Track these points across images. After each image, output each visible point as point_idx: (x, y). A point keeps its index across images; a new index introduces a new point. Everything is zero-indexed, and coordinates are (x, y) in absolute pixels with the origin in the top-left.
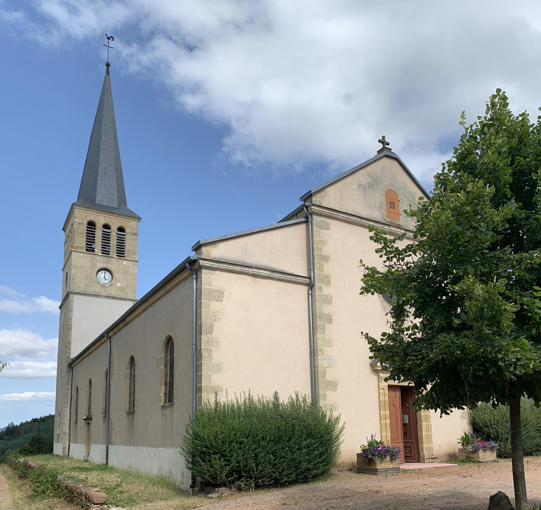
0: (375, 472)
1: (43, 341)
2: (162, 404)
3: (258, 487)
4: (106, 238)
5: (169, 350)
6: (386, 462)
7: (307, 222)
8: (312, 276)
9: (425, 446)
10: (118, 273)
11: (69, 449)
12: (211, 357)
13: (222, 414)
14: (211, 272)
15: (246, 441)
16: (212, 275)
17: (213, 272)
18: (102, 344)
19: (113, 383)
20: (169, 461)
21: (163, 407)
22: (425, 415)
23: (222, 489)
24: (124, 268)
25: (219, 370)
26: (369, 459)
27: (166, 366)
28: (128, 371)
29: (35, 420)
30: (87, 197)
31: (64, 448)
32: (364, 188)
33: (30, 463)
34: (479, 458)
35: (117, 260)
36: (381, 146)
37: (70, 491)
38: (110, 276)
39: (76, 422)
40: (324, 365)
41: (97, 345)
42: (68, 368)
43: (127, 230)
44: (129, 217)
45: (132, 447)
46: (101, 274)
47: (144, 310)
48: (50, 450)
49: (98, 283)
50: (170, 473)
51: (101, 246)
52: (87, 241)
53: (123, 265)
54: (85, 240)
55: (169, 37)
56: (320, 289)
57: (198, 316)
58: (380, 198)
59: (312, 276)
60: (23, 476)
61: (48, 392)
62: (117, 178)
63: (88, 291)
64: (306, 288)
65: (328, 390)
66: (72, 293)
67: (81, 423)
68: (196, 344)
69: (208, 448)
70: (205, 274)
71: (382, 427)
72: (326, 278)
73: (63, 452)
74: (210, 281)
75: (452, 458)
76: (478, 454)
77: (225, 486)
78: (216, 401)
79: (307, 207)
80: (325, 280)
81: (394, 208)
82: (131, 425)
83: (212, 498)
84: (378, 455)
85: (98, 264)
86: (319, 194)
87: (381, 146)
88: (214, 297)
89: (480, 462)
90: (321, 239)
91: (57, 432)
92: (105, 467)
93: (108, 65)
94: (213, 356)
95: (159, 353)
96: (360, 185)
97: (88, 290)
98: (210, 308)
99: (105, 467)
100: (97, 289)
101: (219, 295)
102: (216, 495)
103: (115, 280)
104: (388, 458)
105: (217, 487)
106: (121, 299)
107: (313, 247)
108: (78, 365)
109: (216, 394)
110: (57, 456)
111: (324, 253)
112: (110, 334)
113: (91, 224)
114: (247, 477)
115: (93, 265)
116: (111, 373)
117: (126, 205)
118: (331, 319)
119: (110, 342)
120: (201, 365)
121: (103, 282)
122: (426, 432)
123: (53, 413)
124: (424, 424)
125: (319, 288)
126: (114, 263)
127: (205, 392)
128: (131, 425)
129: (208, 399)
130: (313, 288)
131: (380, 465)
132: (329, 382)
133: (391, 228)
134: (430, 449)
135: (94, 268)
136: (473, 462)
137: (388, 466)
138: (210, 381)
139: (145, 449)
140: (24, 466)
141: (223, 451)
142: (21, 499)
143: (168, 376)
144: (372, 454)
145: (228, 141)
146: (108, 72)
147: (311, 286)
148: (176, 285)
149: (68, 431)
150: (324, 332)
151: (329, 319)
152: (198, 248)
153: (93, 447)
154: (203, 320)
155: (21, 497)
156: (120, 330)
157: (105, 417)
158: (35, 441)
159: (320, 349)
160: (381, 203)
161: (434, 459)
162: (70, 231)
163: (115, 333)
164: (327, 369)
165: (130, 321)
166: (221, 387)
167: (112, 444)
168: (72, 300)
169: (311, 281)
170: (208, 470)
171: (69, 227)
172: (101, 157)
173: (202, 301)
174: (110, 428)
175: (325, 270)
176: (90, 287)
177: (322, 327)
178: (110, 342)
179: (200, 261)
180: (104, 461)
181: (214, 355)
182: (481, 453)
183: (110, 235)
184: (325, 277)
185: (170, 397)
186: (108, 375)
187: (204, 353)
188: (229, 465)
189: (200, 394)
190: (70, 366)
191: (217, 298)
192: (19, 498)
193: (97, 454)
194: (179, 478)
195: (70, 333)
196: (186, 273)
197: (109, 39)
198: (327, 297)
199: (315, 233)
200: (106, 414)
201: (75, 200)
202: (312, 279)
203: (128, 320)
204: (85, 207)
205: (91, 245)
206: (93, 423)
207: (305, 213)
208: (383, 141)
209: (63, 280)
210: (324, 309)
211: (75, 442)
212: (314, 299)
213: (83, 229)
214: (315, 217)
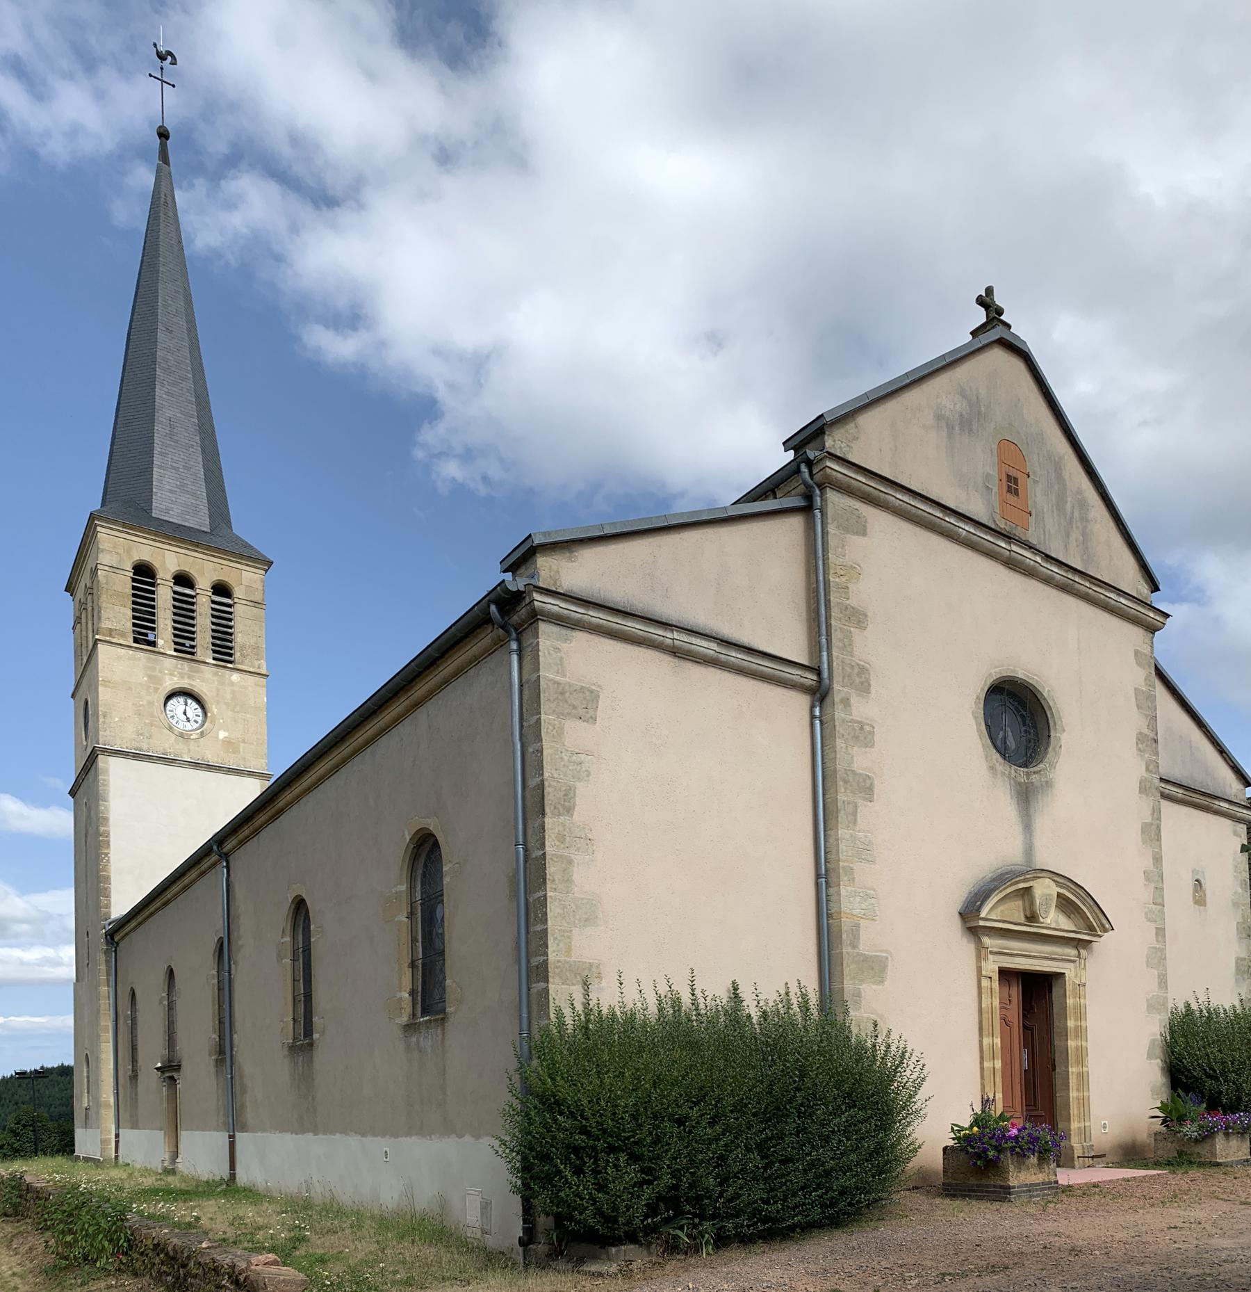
0: (1003, 1194)
1: (17, 900)
2: (405, 1019)
3: (721, 1242)
4: (184, 610)
5: (420, 872)
7: (807, 509)
8: (825, 666)
9: (1075, 1125)
10: (218, 703)
11: (117, 1142)
12: (569, 881)
13: (609, 1040)
14: (564, 631)
15: (694, 1113)
16: (565, 640)
17: (569, 632)
18: (203, 873)
19: (242, 974)
20: (464, 1173)
21: (410, 1028)
22: (1077, 1048)
23: (629, 1249)
24: (233, 692)
25: (589, 920)
26: (978, 1164)
27: (411, 915)
28: (288, 939)
29: (22, 1075)
30: (127, 499)
31: (104, 1142)
32: (950, 428)
33: (28, 1179)
34: (1215, 1155)
35: (215, 669)
36: (980, 316)
37: (173, 1258)
38: (199, 711)
39: (134, 1077)
40: (855, 912)
41: (186, 880)
42: (107, 943)
43: (238, 592)
44: (241, 556)
45: (310, 1135)
46: (177, 705)
47: (336, 768)
48: (66, 1146)
49: (170, 729)
50: (443, 1204)
51: (170, 630)
52: (134, 618)
53: (232, 684)
54: (130, 613)
55: (276, 172)
56: (846, 702)
57: (532, 762)
58: (983, 462)
59: (825, 666)
60: (10, 1211)
61: (32, 1016)
62: (203, 451)
63: (145, 747)
64: (800, 702)
65: (862, 981)
66: (105, 751)
67: (150, 1079)
68: (525, 844)
69: (588, 1134)
70: (548, 638)
71: (987, 1078)
72: (859, 674)
73: (102, 1150)
74: (561, 659)
75: (1130, 1154)
76: (1214, 1145)
77: (632, 1238)
78: (586, 1004)
79: (810, 464)
80: (858, 680)
81: (1016, 493)
82: (305, 1081)
83: (600, 1275)
84: (1012, 1149)
85: (167, 678)
86: (842, 431)
87: (980, 316)
88: (574, 707)
89: (1218, 1165)
91: (82, 1101)
92: (229, 1187)
94: (575, 877)
95: (389, 879)
96: (939, 417)
97: (145, 747)
98: (564, 740)
99: (229, 1187)
100: (164, 743)
101: (585, 703)
102: (614, 1268)
103: (213, 722)
104: (1033, 1160)
105: (614, 1245)
106: (230, 771)
107: (827, 582)
108: (133, 935)
109: (586, 985)
110: (87, 1160)
111: (853, 602)
112: (227, 847)
113: (144, 572)
114: (695, 1215)
115: (155, 680)
116: (234, 948)
117: (231, 528)
118: (870, 789)
119: (228, 867)
120: (543, 902)
121: (183, 726)
122: (1078, 1090)
123: (69, 1061)
125: (842, 701)
126: (206, 679)
127: (557, 980)
128: (305, 1081)
129: (564, 997)
130: (828, 700)
131: (1021, 1176)
132: (866, 959)
133: (1014, 548)
134: (1085, 1133)
135: (156, 690)
136: (1201, 1165)
137: (1034, 1177)
138: (569, 949)
139: (353, 1141)
140: (13, 1188)
141: (635, 1143)
142: (21, 1277)
143: (419, 944)
144: (995, 1148)
145: (429, 436)
147: (819, 694)
148: (446, 682)
149: (112, 1100)
151: (867, 790)
152: (523, 557)
153: (187, 1138)
154: (546, 775)
155: (17, 1269)
156: (256, 832)
157: (220, 1062)
158: (24, 1126)
159: (844, 868)
160: (988, 476)
161: (1097, 1157)
162: (90, 591)
163: (242, 843)
164: (862, 922)
165: (290, 804)
166: (598, 967)
167: (244, 1128)
168: (106, 771)
169: (820, 681)
170: (594, 1200)
171: (85, 580)
172: (159, 391)
173: (543, 717)
174: (237, 1088)
176: (150, 737)
177: (850, 809)
178: (228, 867)
179: (536, 596)
180: (225, 1174)
181: (578, 874)
182: (1220, 1141)
183: (193, 604)
184: (856, 670)
185: (430, 999)
186: (223, 952)
187: (551, 869)
188: (649, 1183)
189: (542, 985)
190: (112, 938)
191: (581, 711)
192: (14, 1274)
193: (202, 1154)
194: (472, 1216)
195: (106, 854)
196: (485, 639)
197: (162, 57)
198: (862, 728)
199: (832, 542)
200: (224, 1053)
201: (96, 505)
202: (825, 675)
203: (281, 803)
204: (124, 526)
205: (146, 635)
206: (184, 1080)
207: (805, 483)
208: (986, 301)
209: (76, 723)
210: (853, 758)
211: (135, 1126)
212: (827, 731)
213: (124, 583)
214: (833, 497)
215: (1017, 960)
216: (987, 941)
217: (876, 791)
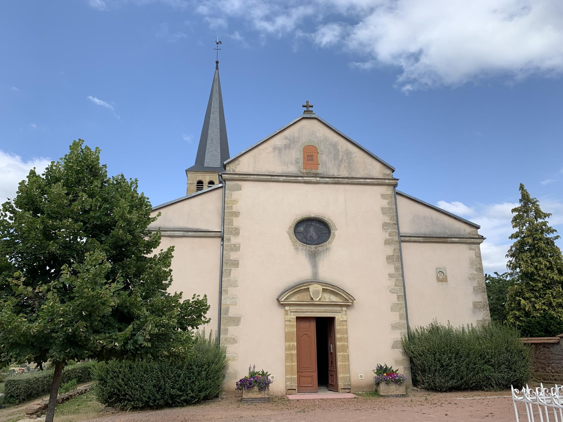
6: (253, 392)
9: (340, 376)
56: (229, 240)
90: (233, 199)
93: (217, 63)
104: (256, 388)
124: (339, 355)
132: (231, 318)
146: (217, 68)
147: (223, 240)
150: (230, 275)
160: (298, 159)
161: (348, 389)
175: (234, 224)
177: (228, 271)
197: (217, 44)
215: (306, 313)
216: (287, 308)
217: (240, 264)
